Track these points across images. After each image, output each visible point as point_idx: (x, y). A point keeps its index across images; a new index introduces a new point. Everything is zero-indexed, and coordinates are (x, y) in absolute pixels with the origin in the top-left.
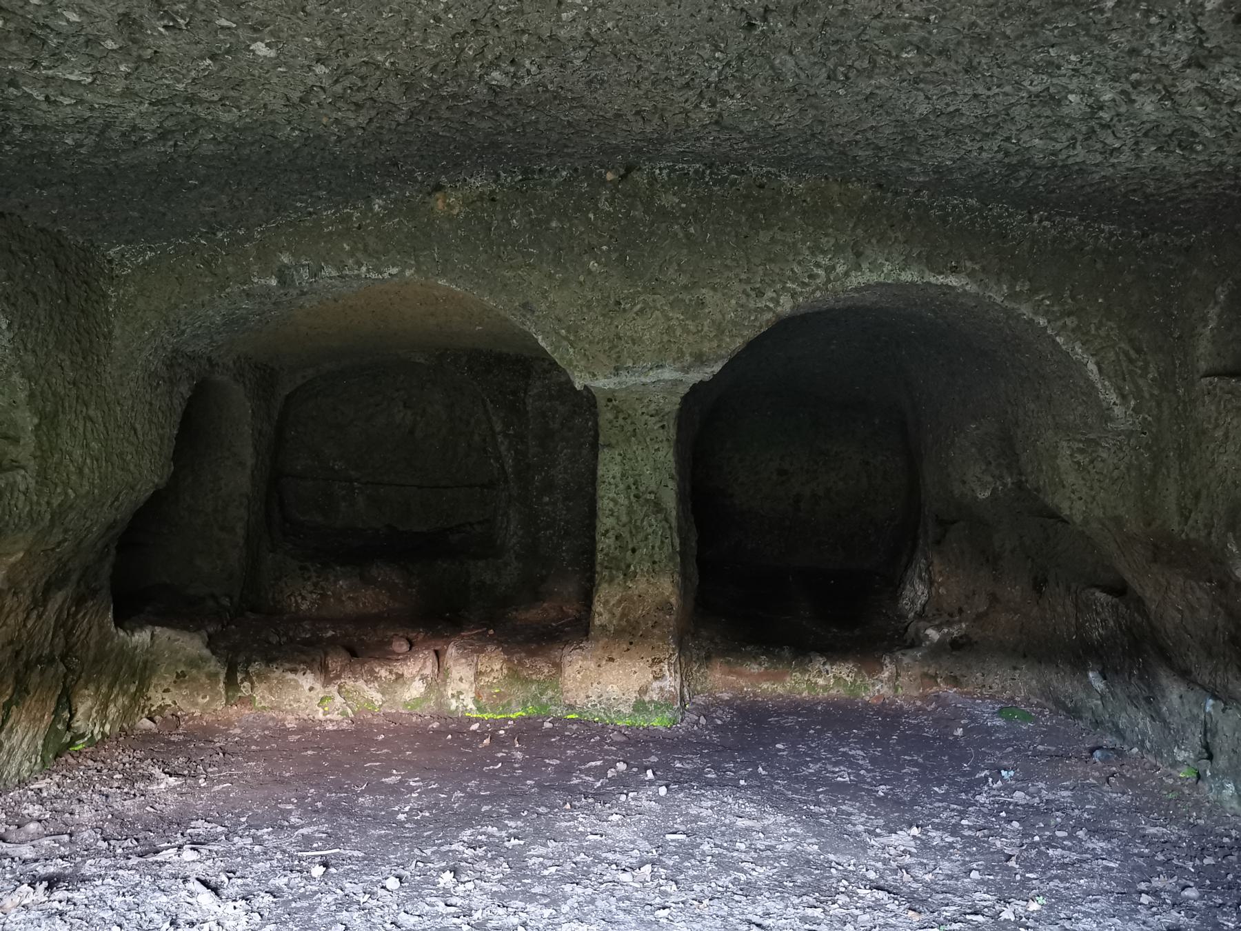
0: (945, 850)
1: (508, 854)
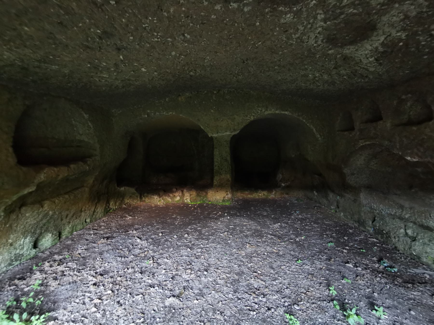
0: (285, 227)
1: (198, 231)
